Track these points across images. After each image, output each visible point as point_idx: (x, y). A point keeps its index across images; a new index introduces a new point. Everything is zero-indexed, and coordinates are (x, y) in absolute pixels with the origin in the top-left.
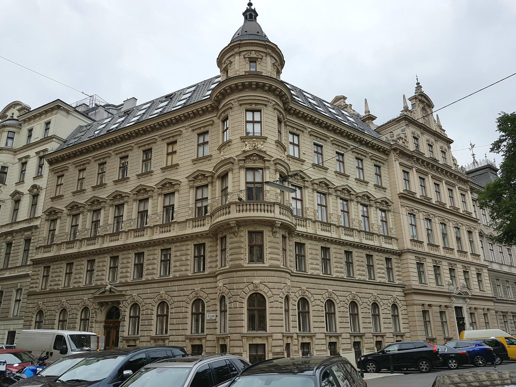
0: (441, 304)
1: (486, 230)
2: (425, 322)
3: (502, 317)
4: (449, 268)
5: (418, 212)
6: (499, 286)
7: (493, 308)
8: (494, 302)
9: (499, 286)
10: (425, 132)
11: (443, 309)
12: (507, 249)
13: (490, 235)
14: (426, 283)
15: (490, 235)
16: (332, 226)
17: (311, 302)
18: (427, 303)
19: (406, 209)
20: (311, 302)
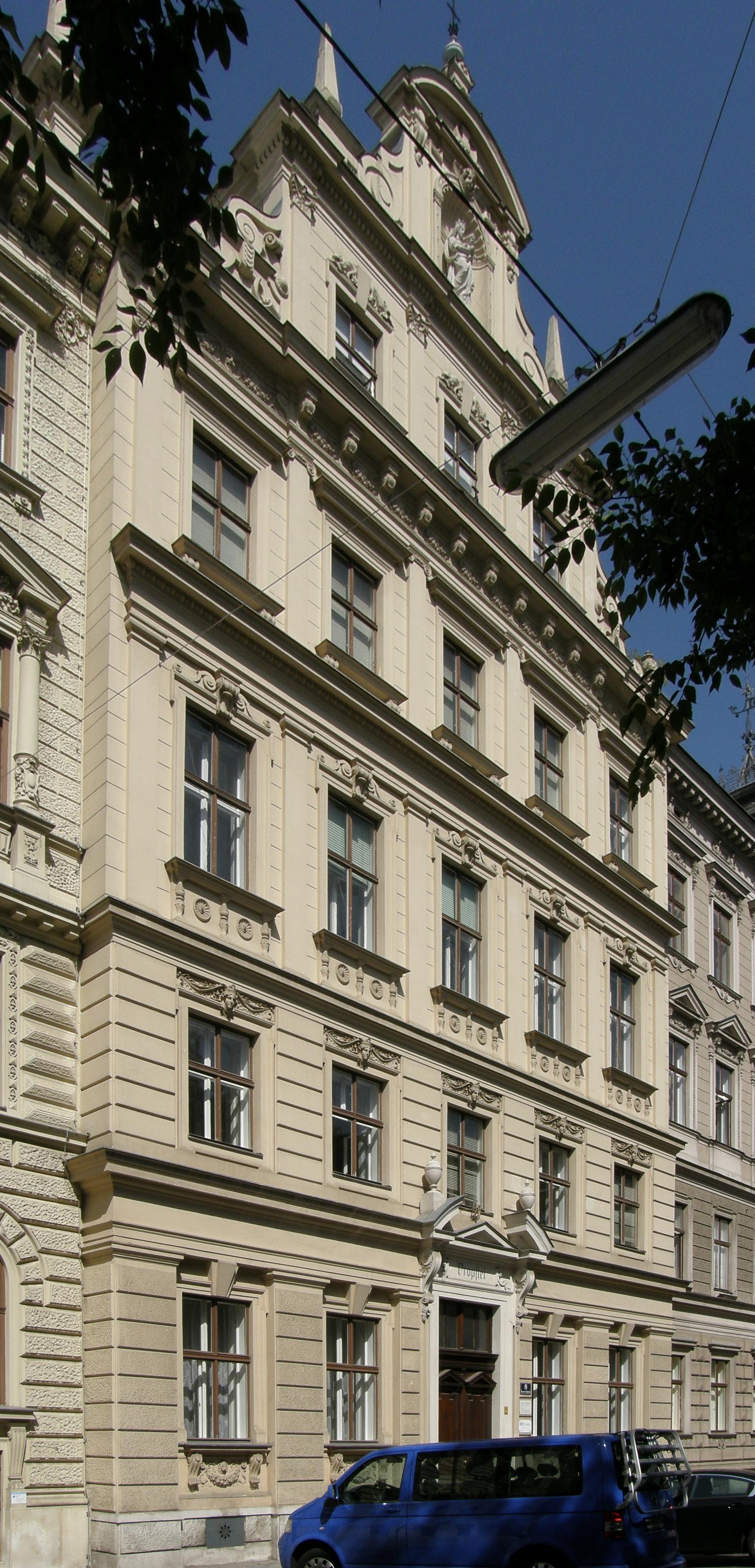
0: (619, 1317)
1: (717, 1005)
2: (615, 1384)
3: (707, 1369)
4: (543, 1140)
5: (649, 967)
6: (727, 1245)
7: (667, 1324)
8: (677, 1307)
9: (727, 1245)
10: (319, 207)
11: (624, 1339)
12: (713, 1067)
13: (730, 1030)
14: (570, 1232)
15: (730, 1030)
16: (21, 829)
17: (9, 1245)
18: (632, 1321)
19: (606, 940)
20: (9, 1245)
